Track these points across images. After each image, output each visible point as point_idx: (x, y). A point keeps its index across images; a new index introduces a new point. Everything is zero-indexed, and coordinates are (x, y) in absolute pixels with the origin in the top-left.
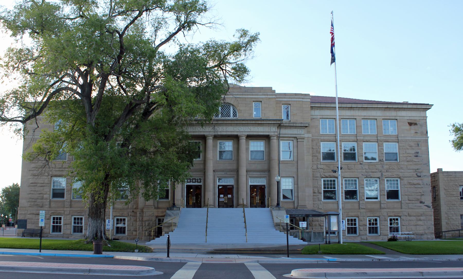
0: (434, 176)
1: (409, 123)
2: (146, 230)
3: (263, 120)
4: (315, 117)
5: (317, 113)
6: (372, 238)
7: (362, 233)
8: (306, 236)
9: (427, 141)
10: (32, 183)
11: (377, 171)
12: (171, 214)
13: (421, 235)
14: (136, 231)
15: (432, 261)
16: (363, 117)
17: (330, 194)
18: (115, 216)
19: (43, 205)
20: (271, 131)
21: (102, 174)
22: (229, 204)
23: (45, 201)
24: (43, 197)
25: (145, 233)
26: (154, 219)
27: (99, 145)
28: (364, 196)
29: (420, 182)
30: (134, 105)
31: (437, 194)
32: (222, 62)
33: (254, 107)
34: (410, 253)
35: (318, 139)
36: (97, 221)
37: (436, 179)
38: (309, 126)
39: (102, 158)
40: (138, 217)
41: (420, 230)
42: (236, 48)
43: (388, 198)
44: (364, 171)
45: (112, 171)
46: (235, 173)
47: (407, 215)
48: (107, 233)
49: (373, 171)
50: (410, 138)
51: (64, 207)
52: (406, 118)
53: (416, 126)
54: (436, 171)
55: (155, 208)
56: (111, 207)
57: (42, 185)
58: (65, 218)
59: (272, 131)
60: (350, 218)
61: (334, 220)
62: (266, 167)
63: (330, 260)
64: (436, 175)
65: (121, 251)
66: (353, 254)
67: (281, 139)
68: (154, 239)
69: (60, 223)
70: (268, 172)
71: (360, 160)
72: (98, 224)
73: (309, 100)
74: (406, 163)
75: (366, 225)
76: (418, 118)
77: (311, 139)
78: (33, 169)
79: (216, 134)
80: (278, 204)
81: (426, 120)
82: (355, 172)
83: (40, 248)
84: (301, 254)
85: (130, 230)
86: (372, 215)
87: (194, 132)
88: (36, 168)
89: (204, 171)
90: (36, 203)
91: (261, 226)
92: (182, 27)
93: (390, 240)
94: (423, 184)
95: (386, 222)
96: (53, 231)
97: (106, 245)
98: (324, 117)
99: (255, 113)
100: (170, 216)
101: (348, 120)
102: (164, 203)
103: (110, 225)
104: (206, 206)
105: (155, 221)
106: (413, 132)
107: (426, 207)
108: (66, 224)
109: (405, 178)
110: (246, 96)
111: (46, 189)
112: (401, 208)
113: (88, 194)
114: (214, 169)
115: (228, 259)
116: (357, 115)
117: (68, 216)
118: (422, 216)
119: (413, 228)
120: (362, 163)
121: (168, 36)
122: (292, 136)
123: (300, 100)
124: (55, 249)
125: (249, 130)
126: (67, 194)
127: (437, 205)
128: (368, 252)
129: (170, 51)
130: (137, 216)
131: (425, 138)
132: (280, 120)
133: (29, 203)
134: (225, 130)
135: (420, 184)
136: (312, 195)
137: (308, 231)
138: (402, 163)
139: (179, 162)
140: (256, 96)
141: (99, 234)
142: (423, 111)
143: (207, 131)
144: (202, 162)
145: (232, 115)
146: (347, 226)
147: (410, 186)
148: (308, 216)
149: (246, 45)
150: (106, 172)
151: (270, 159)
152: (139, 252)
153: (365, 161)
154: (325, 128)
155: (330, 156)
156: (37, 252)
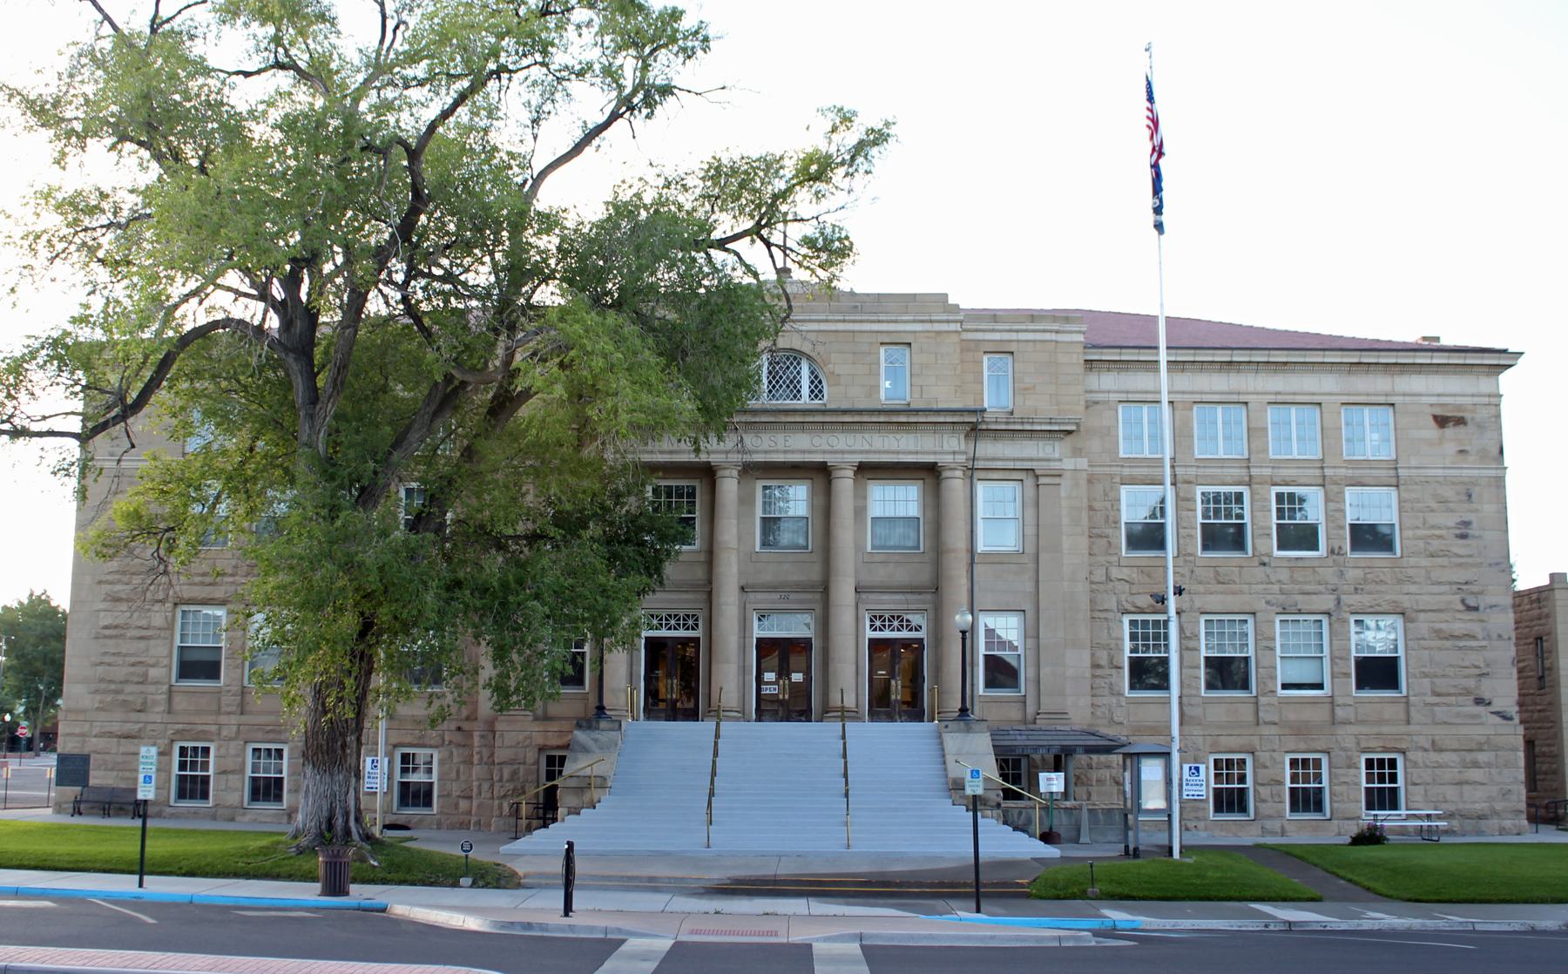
0: (1538, 600)
1: (1435, 417)
2: (505, 796)
3: (917, 411)
4: (1100, 397)
5: (1108, 381)
6: (1301, 830)
7: (1266, 809)
8: (1061, 823)
9: (1499, 483)
10: (106, 627)
11: (1321, 588)
12: (590, 743)
13: (1480, 818)
14: (470, 798)
15: (1474, 931)
16: (1272, 398)
17: (1149, 673)
18: (395, 746)
19: (144, 703)
20: (945, 448)
21: (349, 623)
22: (795, 707)
23: (151, 688)
24: (146, 675)
25: (500, 807)
26: (531, 755)
27: (339, 523)
28: (1274, 678)
29: (1476, 628)
30: (456, 383)
31: (1547, 663)
32: (767, 217)
33: (883, 365)
34: (1411, 896)
35: (1111, 476)
36: (331, 775)
37: (1545, 610)
38: (1078, 431)
39: (349, 566)
40: (476, 750)
41: (1476, 800)
42: (816, 170)
43: (1360, 686)
44: (1276, 588)
45: (383, 610)
46: (818, 596)
47: (1428, 745)
48: (367, 818)
49: (1307, 588)
50: (1440, 472)
51: (219, 712)
52: (1424, 400)
53: (1461, 429)
54: (1544, 581)
55: (536, 719)
56: (382, 725)
57: (144, 633)
58: (223, 751)
59: (946, 448)
60: (1225, 757)
61: (1151, 771)
62: (924, 576)
63: (1119, 925)
64: (1544, 595)
65: (413, 884)
66: (1209, 899)
67: (977, 475)
68: (529, 829)
69: (205, 766)
70: (935, 589)
71: (1262, 549)
72: (336, 788)
73: (1080, 338)
74: (1425, 562)
75: (1281, 783)
76: (1468, 400)
77: (1084, 475)
78: (110, 578)
79: (747, 458)
80: (964, 711)
81: (1498, 405)
82: (1241, 592)
83: (141, 867)
84: (1028, 896)
85: (449, 795)
86: (1302, 746)
87: (671, 452)
88: (124, 573)
89: (708, 590)
90: (121, 697)
91: (903, 790)
92: (624, 107)
93: (1358, 840)
94: (1488, 637)
95: (1353, 771)
96: (182, 795)
97: (363, 860)
98: (1131, 397)
99: (887, 384)
100: (585, 750)
101: (1219, 408)
102: (570, 701)
103: (377, 774)
104: (716, 713)
105: (537, 762)
106: (1451, 448)
107: (1498, 720)
108: (224, 772)
109: (1422, 616)
110: (857, 327)
111: (158, 649)
112: (1408, 723)
113: (303, 690)
114: (743, 582)
115: (768, 925)
116: (1251, 389)
117: (233, 744)
118: (1481, 750)
119: (1451, 792)
120: (1266, 560)
121: (578, 135)
122: (1019, 465)
123: (1047, 336)
124: (191, 874)
125: (867, 447)
126: (227, 666)
127: (1550, 704)
128: (1258, 893)
129: (578, 197)
130: (471, 747)
131: (1493, 473)
132: (974, 412)
133: (98, 697)
134: (781, 447)
135: (1474, 637)
136: (1088, 674)
137: (1068, 804)
138: (1412, 561)
139: (609, 580)
140: (891, 327)
141: (339, 822)
142: (1488, 374)
143: (717, 450)
144: (702, 558)
145: (805, 391)
146: (1212, 785)
147: (1438, 643)
148: (1069, 751)
149: (853, 158)
150: (362, 614)
151: (938, 550)
152: (474, 885)
153: (1277, 553)
154: (1142, 433)
155: (1149, 537)
156: (125, 884)
